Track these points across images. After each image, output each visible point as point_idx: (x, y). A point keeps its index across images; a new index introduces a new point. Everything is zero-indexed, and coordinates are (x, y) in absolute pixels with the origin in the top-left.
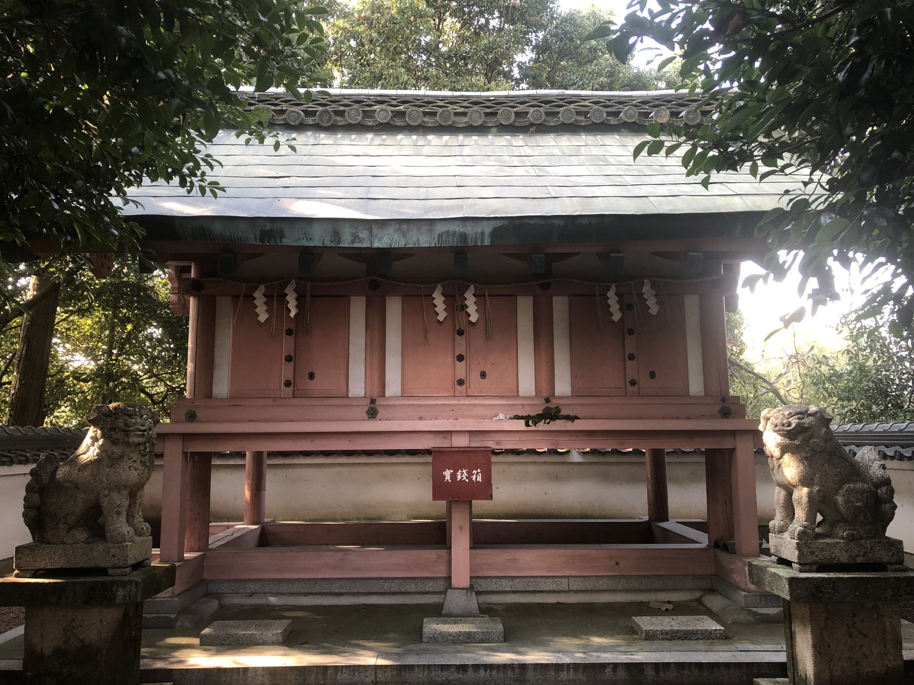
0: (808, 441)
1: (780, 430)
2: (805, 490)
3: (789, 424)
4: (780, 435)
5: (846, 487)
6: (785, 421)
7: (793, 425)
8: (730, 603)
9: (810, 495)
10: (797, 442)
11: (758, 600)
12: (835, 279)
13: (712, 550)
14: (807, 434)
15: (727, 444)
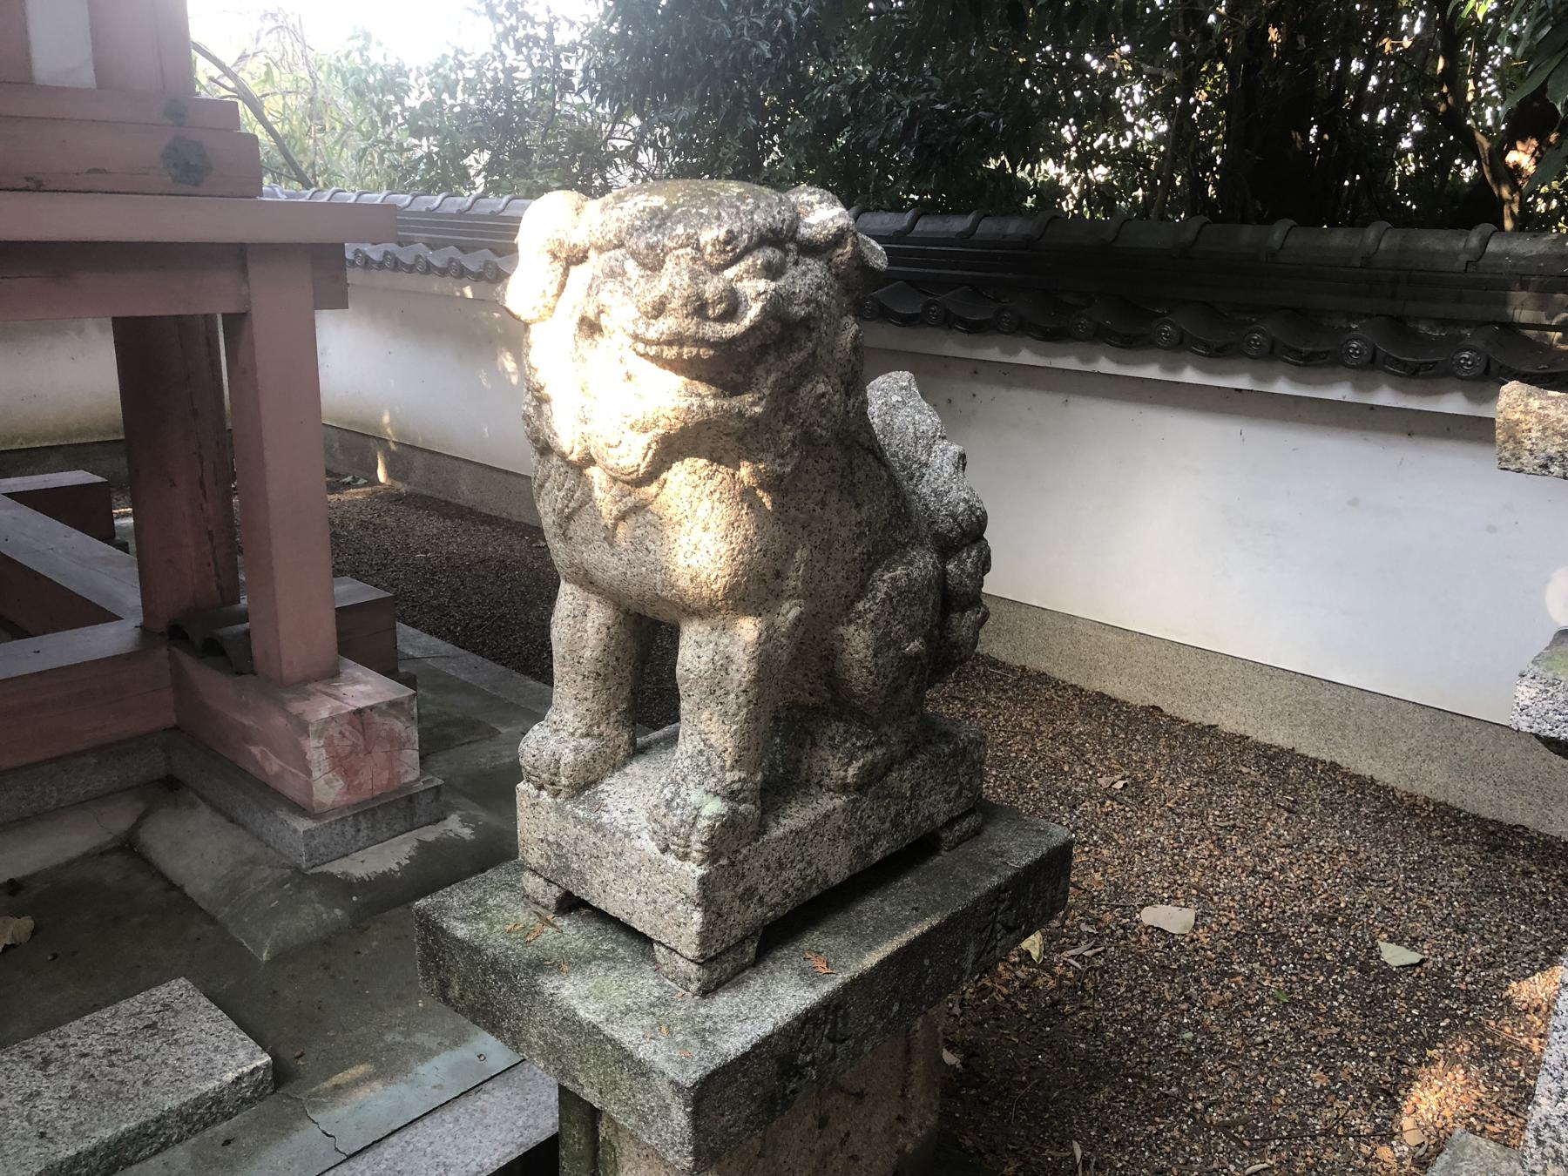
0: (793, 390)
1: (677, 340)
2: (748, 629)
3: (733, 308)
4: (676, 366)
5: (885, 580)
6: (712, 287)
7: (753, 312)
8: (251, 849)
9: (767, 640)
10: (751, 404)
11: (350, 831)
12: (190, 22)
13: (164, 651)
14: (797, 357)
15: (212, 298)
